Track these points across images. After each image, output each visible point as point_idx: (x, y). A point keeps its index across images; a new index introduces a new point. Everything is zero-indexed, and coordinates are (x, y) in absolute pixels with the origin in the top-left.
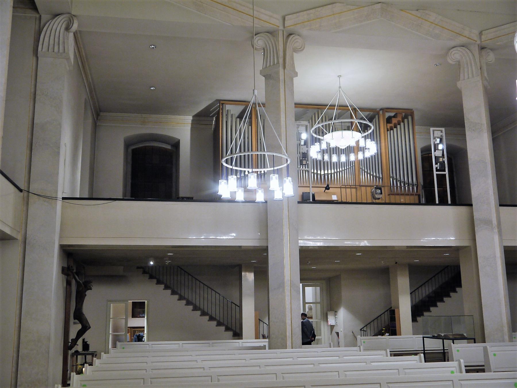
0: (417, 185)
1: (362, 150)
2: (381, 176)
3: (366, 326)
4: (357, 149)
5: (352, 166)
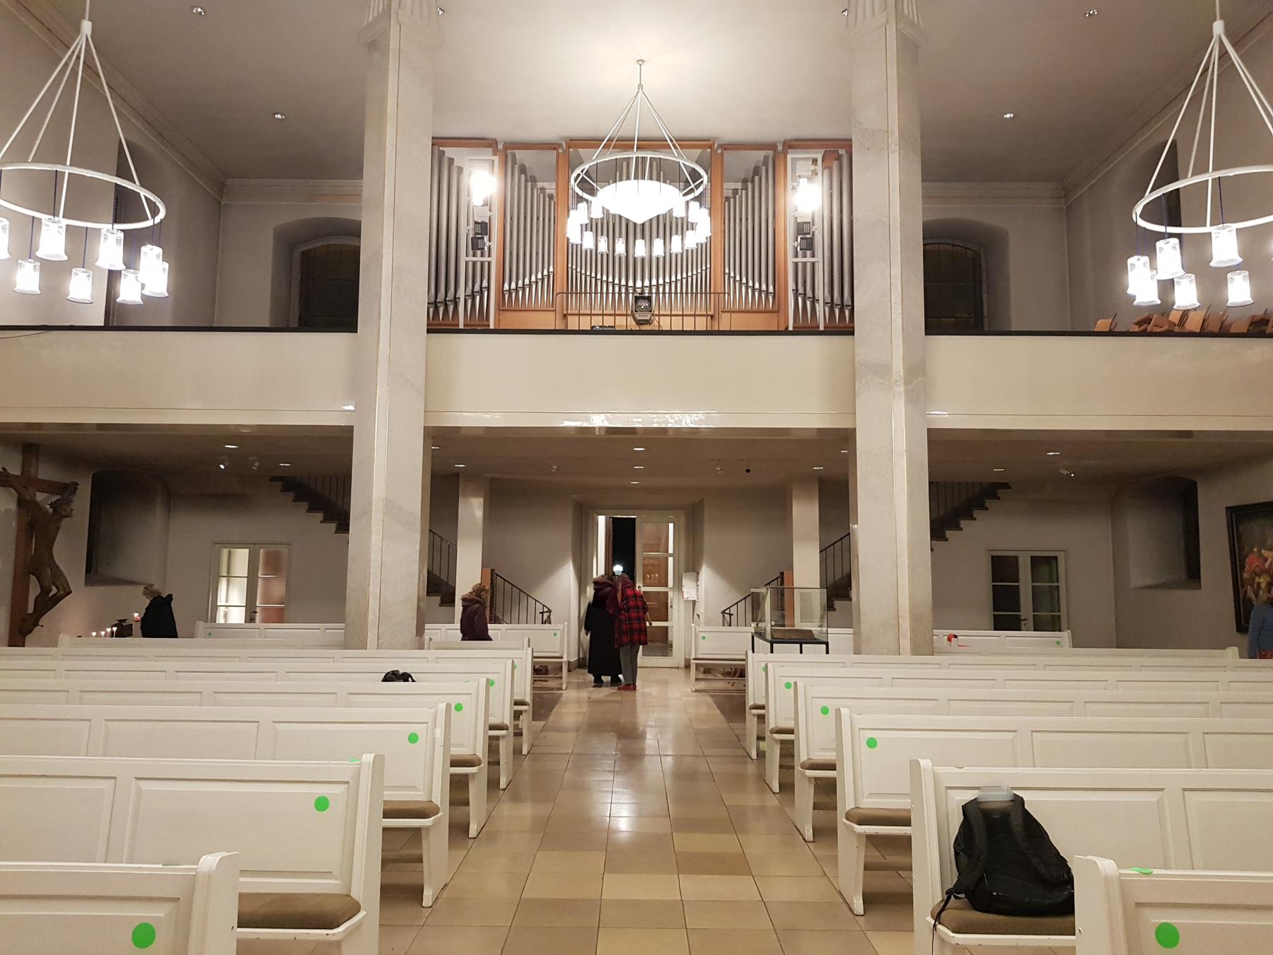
0: (850, 307)
1: (689, 225)
2: (771, 289)
3: (745, 598)
4: (665, 226)
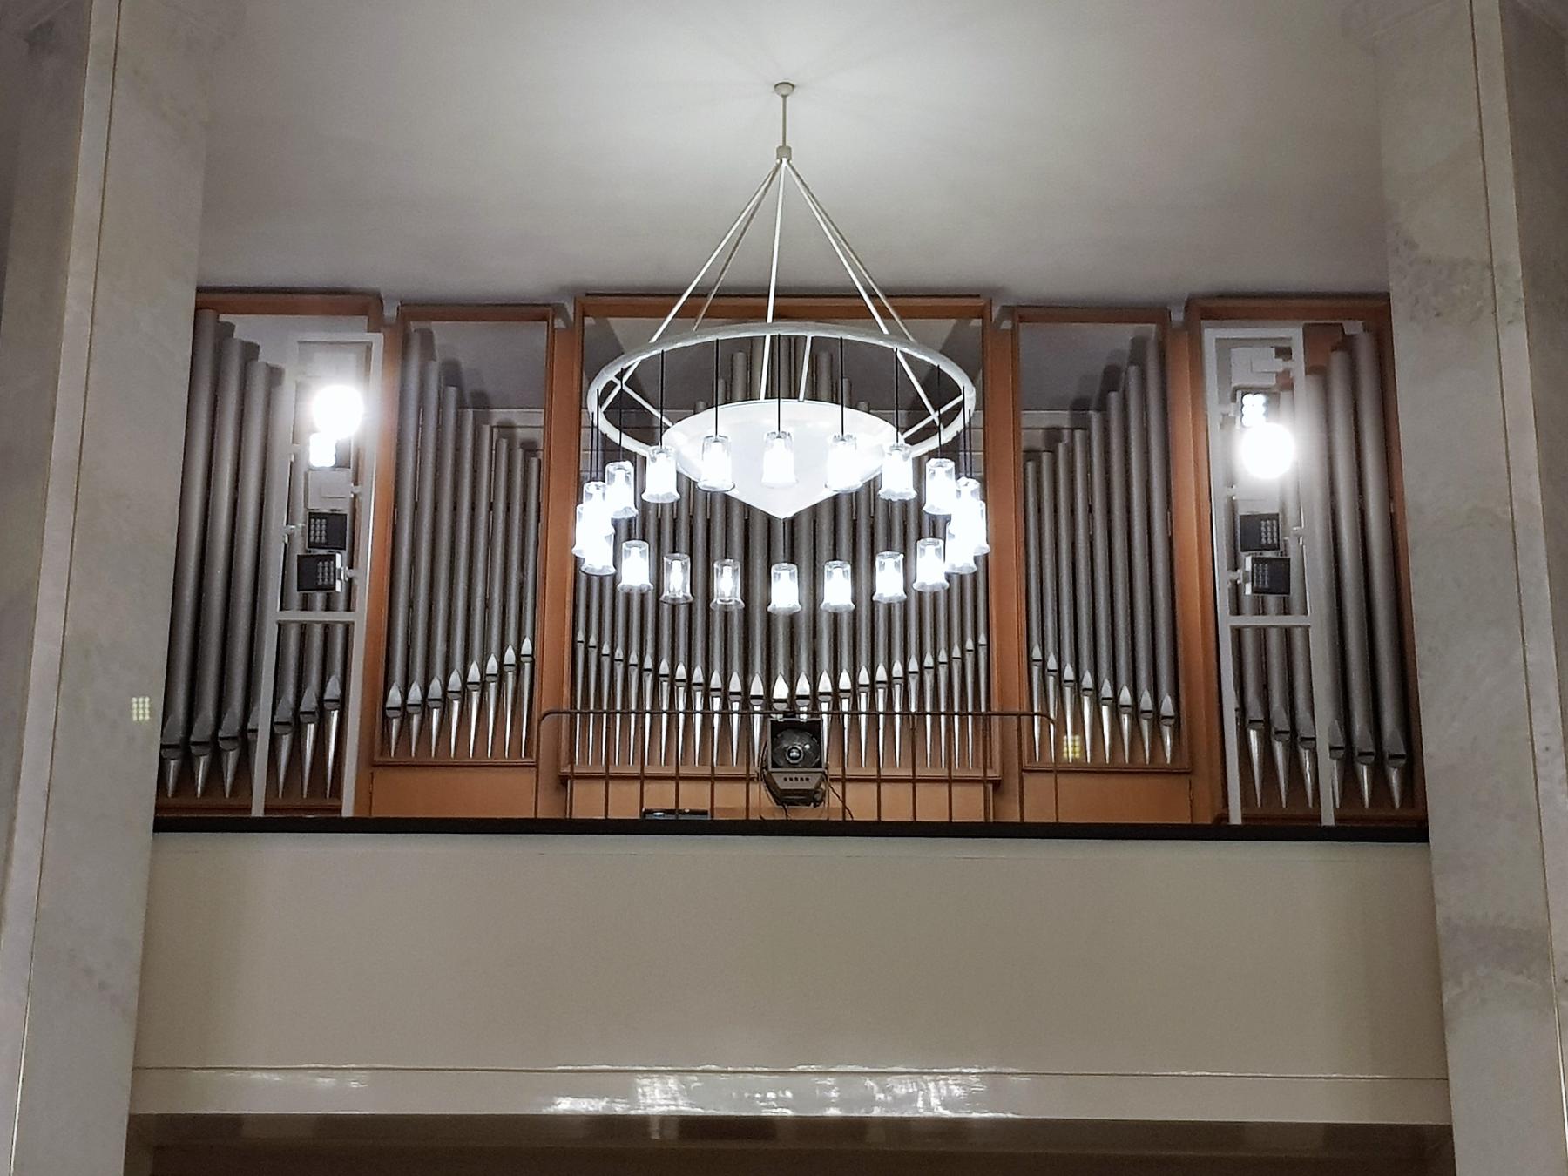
5: (969, 645)
